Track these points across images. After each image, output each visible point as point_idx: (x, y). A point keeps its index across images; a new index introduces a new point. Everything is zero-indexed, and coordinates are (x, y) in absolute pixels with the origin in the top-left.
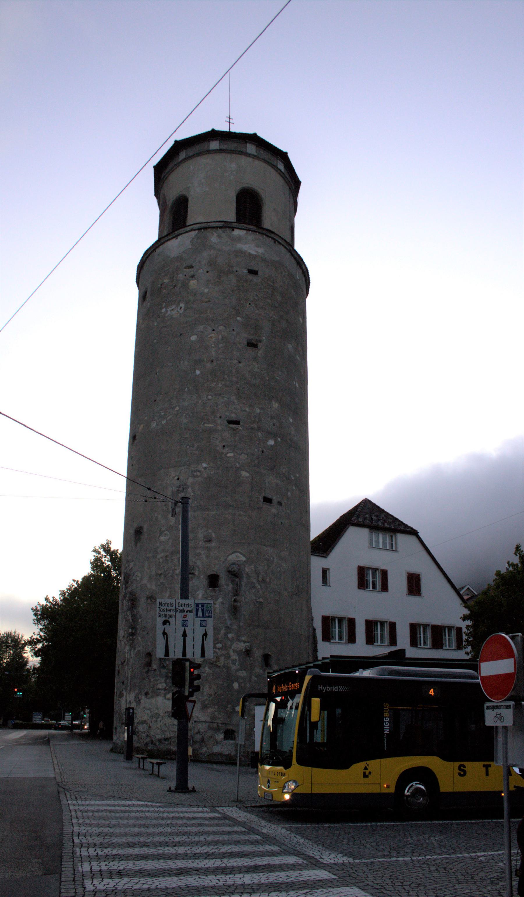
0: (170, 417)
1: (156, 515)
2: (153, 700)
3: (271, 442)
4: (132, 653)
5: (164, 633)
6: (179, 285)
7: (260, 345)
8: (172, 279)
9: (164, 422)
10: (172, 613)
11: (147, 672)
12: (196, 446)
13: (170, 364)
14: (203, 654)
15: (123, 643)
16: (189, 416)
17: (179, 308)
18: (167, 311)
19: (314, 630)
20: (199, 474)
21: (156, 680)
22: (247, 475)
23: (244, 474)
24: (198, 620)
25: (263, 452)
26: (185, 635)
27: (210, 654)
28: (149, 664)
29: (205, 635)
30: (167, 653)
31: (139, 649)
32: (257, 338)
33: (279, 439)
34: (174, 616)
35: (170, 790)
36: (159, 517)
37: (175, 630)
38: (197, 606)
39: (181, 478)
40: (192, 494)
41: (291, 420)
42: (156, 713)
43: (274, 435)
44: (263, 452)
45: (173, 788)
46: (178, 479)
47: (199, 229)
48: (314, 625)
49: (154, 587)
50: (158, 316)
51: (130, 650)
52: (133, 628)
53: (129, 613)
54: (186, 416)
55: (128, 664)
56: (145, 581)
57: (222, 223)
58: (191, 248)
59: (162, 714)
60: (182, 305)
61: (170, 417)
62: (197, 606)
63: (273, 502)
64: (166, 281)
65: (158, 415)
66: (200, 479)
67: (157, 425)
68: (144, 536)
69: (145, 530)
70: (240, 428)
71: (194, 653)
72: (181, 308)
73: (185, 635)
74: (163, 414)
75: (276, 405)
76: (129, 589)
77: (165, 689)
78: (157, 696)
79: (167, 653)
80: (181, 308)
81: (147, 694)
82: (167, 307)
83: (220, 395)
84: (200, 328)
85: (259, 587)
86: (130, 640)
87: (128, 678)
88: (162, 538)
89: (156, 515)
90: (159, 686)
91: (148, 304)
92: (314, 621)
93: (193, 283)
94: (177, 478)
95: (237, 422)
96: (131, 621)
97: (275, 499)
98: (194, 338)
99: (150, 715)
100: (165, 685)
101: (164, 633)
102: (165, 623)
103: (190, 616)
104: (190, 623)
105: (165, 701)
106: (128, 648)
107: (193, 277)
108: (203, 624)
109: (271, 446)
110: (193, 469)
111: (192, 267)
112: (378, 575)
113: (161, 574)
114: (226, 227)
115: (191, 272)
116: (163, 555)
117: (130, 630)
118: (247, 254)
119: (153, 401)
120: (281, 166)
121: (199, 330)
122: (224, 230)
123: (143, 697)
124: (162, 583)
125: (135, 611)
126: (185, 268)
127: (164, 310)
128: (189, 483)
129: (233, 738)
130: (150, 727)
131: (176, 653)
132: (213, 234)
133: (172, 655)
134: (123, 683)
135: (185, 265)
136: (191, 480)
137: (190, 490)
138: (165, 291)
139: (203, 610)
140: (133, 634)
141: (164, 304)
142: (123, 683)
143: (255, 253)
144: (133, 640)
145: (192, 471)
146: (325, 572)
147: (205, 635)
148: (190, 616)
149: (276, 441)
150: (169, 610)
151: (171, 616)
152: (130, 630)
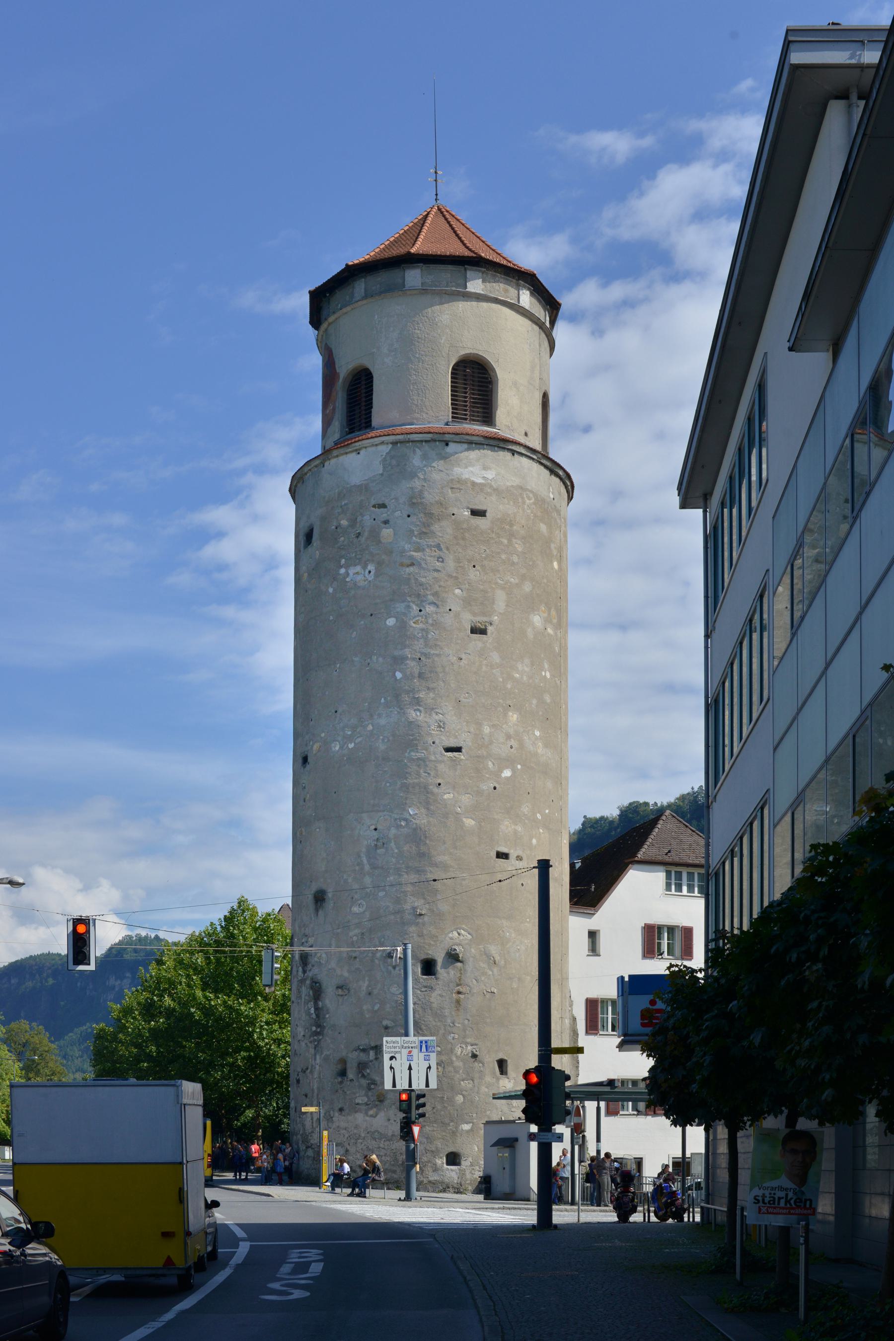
0: (360, 739)
1: (345, 877)
2: (350, 1118)
3: (507, 773)
4: (318, 1057)
5: (391, 1068)
6: (366, 534)
7: (490, 629)
8: (353, 522)
9: (351, 746)
10: (397, 1050)
11: (341, 1083)
12: (399, 783)
13: (356, 659)
14: (427, 1085)
15: (303, 1044)
16: (389, 740)
17: (367, 572)
18: (347, 574)
19: (574, 1019)
20: (403, 823)
21: (355, 1094)
22: (473, 822)
23: (469, 822)
24: (422, 1055)
25: (495, 788)
26: (410, 1068)
27: (433, 1085)
28: (343, 1073)
29: (429, 1067)
30: (394, 1085)
31: (328, 1053)
32: (485, 619)
33: (519, 767)
34: (400, 1052)
35: (400, 1200)
36: (350, 880)
37: (400, 1065)
38: (421, 1042)
39: (379, 827)
40: (396, 851)
41: (537, 733)
42: (355, 1134)
43: (509, 762)
44: (495, 788)
45: (403, 1198)
46: (376, 829)
47: (394, 443)
48: (574, 1012)
49: (346, 974)
50: (335, 579)
51: (315, 1055)
52: (318, 1026)
53: (311, 1005)
54: (383, 740)
55: (311, 1072)
56: (333, 964)
57: (430, 435)
58: (382, 475)
59: (363, 1135)
60: (371, 567)
61: (360, 739)
62: (421, 1042)
63: (510, 856)
64: (344, 523)
65: (341, 733)
66: (405, 831)
67: (341, 748)
68: (329, 905)
69: (330, 895)
70: (462, 757)
71: (419, 1085)
72: (370, 572)
73: (410, 1068)
74: (349, 733)
75: (514, 717)
76: (310, 974)
77: (367, 1104)
78: (356, 1112)
79: (394, 1085)
80: (370, 572)
81: (341, 1110)
82: (347, 567)
83: (433, 709)
84: (400, 607)
85: (491, 973)
86: (315, 1041)
87: (313, 1090)
88: (355, 909)
89: (345, 877)
90: (358, 1101)
91: (315, 550)
92: (574, 1007)
93: (387, 533)
94: (373, 827)
95: (458, 750)
96: (314, 1016)
97: (513, 854)
98: (391, 622)
99: (347, 1136)
100: (366, 1099)
101: (391, 1068)
102: (392, 1058)
103: (415, 1052)
104: (415, 1058)
105: (367, 1118)
106: (312, 1051)
107: (386, 522)
108: (427, 1059)
109: (507, 778)
110: (396, 816)
111: (383, 506)
112: (678, 936)
113: (355, 958)
114: (435, 441)
115: (383, 514)
116: (357, 931)
117: (314, 1028)
118: (469, 485)
119: (333, 711)
120: (526, 299)
121: (398, 610)
122: (432, 444)
123: (337, 1114)
124: (358, 969)
125: (320, 1004)
126: (374, 506)
127: (343, 571)
128: (391, 835)
129: (458, 1164)
130: (347, 1151)
131: (402, 1084)
132: (414, 451)
133: (398, 1087)
134: (306, 1096)
135: (373, 502)
136: (393, 831)
137: (392, 844)
138: (342, 539)
139: (426, 1046)
140: (316, 1033)
141: (343, 561)
142: (306, 1096)
143: (482, 481)
144: (319, 1041)
145: (396, 819)
146: (593, 935)
147: (429, 1067)
148: (415, 1052)
149: (514, 771)
150: (395, 1047)
151: (397, 1052)
152: (314, 1028)
